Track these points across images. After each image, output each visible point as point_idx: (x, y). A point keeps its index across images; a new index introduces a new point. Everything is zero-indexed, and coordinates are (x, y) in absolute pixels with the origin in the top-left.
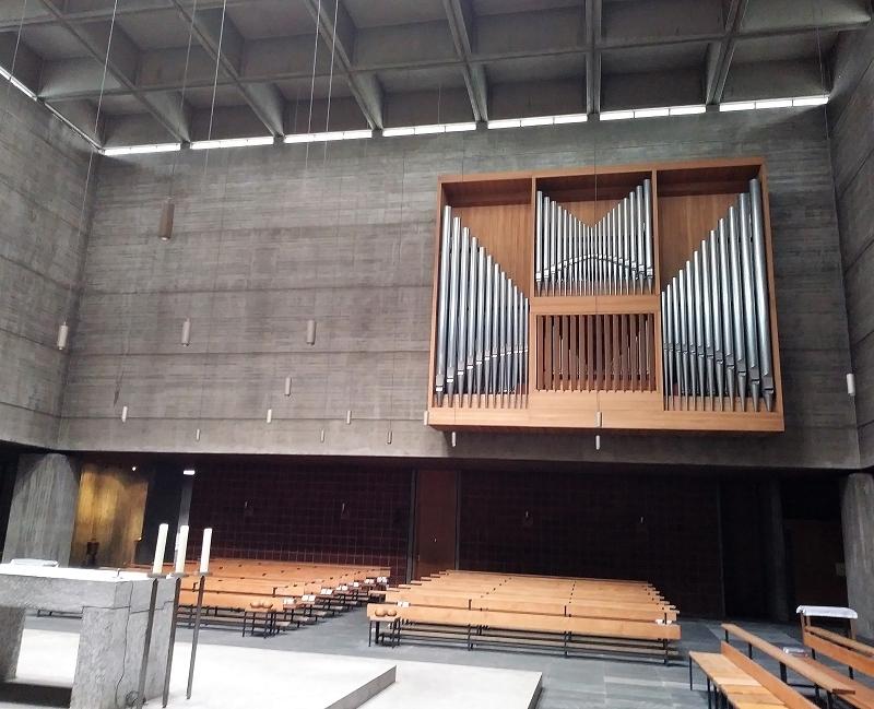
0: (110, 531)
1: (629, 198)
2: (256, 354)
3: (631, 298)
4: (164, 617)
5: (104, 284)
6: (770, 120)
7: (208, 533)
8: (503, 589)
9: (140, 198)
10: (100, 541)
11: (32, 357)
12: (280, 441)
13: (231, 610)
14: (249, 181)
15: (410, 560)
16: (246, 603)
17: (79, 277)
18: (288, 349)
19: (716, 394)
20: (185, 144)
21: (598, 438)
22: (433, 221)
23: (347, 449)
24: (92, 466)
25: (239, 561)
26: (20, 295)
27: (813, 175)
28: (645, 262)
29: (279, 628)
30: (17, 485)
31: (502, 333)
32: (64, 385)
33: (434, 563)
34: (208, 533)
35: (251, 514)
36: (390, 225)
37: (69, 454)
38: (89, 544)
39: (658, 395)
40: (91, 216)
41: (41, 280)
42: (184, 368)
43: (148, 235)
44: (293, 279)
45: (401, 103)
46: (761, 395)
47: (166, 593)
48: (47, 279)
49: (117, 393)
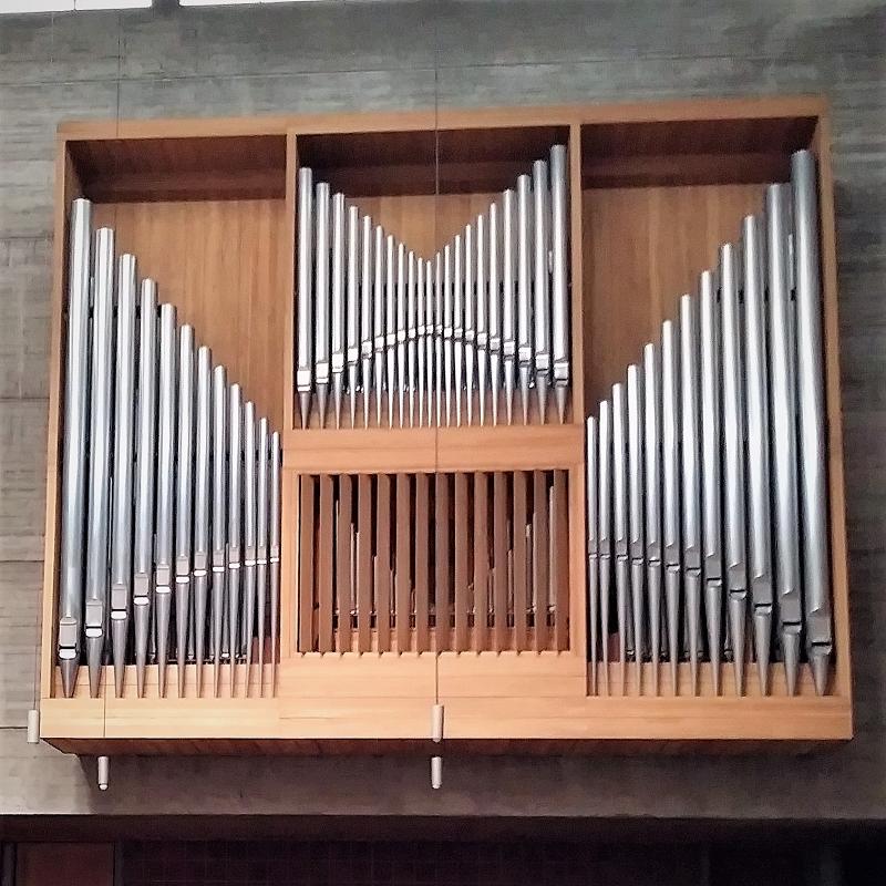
1: (531, 174)
21: (436, 762)
39: (575, 660)
46: (803, 657)
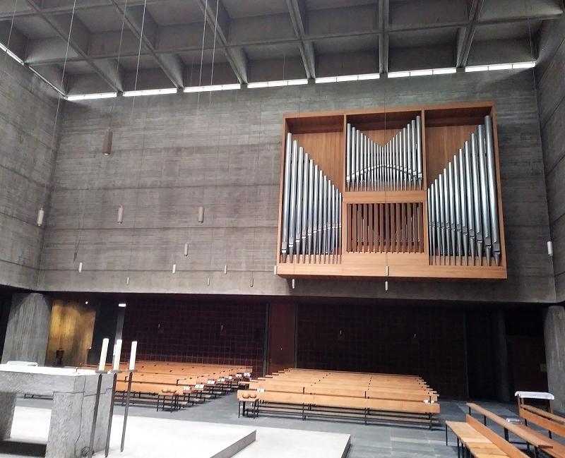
0: (71, 343)
1: (406, 128)
2: (166, 229)
3: (408, 192)
4: (106, 398)
5: (67, 183)
6: (498, 78)
7: (134, 344)
8: (325, 381)
9: (90, 128)
10: (65, 349)
11: (21, 230)
12: (181, 285)
13: (150, 394)
14: (161, 117)
15: (265, 362)
16: (159, 389)
17: (51, 179)
18: (186, 225)
19: (463, 255)
20: (120, 93)
21: (386, 283)
22: (280, 143)
23: (224, 290)
24: (59, 301)
25: (155, 362)
26: (13, 191)
27: (526, 113)
28: (417, 169)
29: (180, 406)
30: (11, 313)
31: (324, 215)
32: (41, 249)
33: (280, 364)
34: (134, 344)
35: (162, 332)
36: (252, 145)
37: (45, 293)
38: (58, 352)
39: (425, 255)
40: (59, 139)
41: (26, 181)
42: (119, 238)
43: (96, 152)
44: (189, 180)
45: (259, 67)
46: (492, 255)
47: (107, 383)
48: (30, 180)
49: (76, 254)
